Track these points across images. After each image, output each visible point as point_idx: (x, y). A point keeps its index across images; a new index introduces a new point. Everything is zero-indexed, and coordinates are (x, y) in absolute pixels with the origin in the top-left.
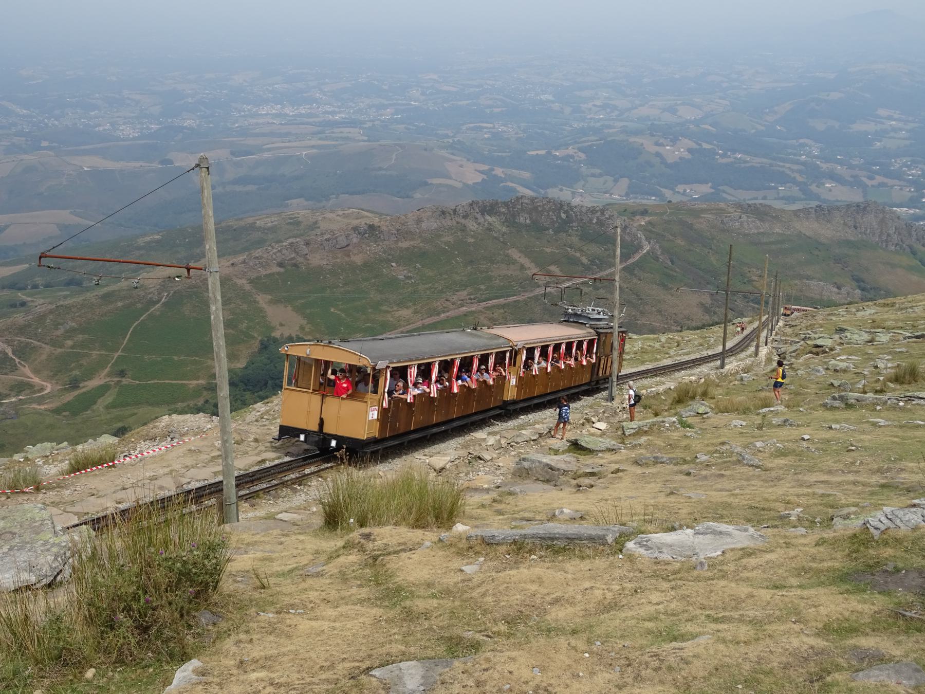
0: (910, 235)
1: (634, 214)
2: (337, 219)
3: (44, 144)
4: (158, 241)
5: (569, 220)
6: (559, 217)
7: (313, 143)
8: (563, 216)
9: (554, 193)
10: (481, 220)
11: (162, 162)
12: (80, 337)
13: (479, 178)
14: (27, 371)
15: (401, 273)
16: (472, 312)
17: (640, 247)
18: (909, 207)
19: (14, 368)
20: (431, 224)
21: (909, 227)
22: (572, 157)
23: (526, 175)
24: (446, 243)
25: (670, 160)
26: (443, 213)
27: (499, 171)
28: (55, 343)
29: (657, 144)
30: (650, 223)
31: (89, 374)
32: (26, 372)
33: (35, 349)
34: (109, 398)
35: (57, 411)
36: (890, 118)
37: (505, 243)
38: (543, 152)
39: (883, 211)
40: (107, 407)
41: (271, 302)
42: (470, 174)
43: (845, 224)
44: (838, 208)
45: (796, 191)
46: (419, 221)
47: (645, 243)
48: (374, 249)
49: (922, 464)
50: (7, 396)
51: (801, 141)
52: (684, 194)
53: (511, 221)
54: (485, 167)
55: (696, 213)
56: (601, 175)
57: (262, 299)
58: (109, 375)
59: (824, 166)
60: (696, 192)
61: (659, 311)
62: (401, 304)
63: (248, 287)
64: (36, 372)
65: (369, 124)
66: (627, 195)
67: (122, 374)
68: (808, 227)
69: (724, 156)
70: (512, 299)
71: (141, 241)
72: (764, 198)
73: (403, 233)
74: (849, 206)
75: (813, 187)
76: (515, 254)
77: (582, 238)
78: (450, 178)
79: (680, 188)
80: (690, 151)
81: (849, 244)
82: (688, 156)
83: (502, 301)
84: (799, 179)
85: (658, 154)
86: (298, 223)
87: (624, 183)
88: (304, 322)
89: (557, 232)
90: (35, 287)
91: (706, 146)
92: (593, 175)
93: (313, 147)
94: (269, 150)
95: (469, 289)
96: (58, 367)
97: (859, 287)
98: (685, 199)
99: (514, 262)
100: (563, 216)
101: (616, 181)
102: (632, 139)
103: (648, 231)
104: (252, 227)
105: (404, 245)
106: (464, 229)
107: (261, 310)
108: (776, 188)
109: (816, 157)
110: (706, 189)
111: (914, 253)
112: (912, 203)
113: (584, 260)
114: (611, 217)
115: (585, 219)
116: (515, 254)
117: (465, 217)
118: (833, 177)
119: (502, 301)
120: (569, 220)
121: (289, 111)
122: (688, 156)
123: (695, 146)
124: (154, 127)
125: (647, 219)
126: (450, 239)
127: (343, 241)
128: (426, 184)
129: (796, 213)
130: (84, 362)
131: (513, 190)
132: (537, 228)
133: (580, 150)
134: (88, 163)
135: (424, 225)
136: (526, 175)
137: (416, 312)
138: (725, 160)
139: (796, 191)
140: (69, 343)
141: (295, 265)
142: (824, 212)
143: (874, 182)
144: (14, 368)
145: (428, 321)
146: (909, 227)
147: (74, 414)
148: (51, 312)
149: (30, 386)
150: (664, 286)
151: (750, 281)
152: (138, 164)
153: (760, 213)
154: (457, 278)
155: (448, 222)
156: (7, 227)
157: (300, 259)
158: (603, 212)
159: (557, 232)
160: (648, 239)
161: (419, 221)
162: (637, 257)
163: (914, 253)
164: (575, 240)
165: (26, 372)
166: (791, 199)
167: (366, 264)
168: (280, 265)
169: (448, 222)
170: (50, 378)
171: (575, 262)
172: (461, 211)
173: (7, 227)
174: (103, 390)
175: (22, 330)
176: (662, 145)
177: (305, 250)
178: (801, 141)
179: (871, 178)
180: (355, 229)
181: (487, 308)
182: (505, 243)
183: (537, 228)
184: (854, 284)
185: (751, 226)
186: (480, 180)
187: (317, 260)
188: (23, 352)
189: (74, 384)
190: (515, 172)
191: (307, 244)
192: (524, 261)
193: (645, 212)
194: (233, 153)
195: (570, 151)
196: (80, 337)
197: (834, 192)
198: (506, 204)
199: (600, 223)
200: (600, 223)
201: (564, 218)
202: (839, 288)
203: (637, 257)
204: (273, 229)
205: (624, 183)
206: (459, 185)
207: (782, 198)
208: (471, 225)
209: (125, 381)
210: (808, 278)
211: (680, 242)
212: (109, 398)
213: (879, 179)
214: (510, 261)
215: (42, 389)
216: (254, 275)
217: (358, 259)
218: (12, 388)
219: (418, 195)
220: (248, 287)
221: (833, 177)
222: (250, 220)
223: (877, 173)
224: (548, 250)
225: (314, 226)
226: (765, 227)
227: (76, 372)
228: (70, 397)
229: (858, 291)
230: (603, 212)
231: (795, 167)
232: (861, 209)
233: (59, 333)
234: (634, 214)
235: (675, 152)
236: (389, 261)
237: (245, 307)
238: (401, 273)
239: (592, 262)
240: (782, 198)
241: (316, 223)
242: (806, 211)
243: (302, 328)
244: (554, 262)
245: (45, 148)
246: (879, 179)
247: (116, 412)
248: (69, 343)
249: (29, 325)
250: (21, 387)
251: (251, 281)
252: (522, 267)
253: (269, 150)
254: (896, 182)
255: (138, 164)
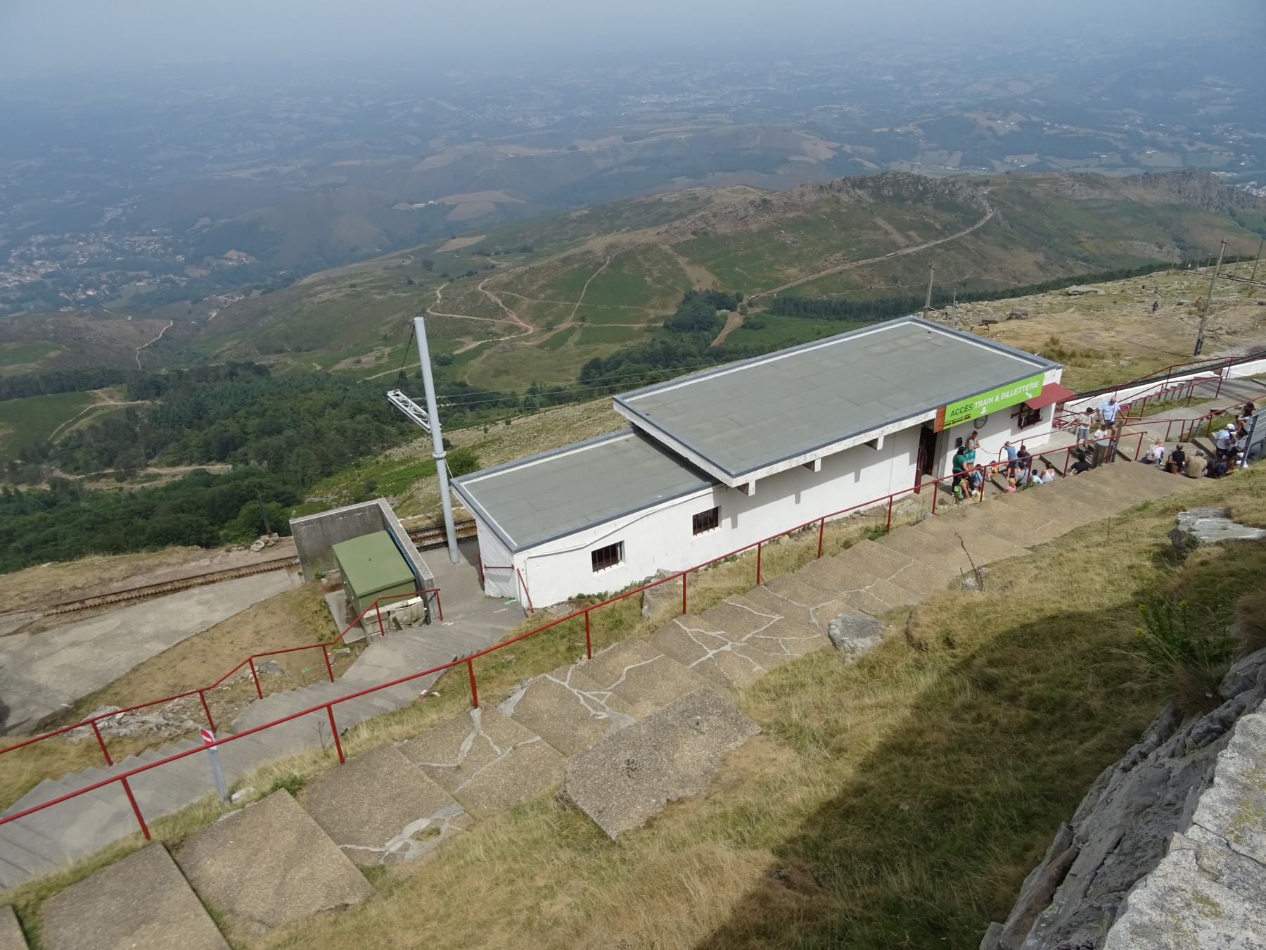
0: (1231, 198)
1: (977, 184)
2: (732, 193)
3: (474, 136)
4: (587, 216)
5: (925, 192)
6: (917, 189)
7: (689, 127)
8: (920, 188)
9: (895, 166)
10: (852, 193)
11: (569, 149)
12: (549, 292)
13: (830, 154)
14: (514, 316)
15: (788, 238)
16: (846, 271)
17: (985, 214)
18: (1227, 171)
19: (505, 315)
20: (811, 198)
21: (1231, 190)
22: (912, 133)
23: (871, 150)
24: (824, 213)
25: (1001, 134)
26: (821, 187)
27: (848, 148)
28: (531, 296)
29: (990, 118)
30: (992, 192)
31: (560, 319)
32: (514, 318)
33: (517, 300)
34: (576, 337)
35: (541, 346)
36: (1216, 85)
37: (872, 213)
38: (886, 130)
39: (1208, 176)
40: (576, 344)
41: (689, 263)
42: (824, 151)
43: (1170, 189)
44: (1164, 175)
45: (1117, 159)
46: (802, 195)
47: (988, 209)
48: (767, 219)
49: (723, 949)
50: (502, 336)
51: (1126, 110)
52: (1012, 164)
53: (876, 194)
54: (836, 145)
55: (1033, 183)
56: (937, 149)
57: (682, 261)
58: (574, 320)
59: (1147, 134)
60: (1024, 161)
61: (1000, 269)
62: (790, 264)
63: (670, 252)
64: (521, 317)
65: (734, 110)
66: (960, 166)
67: (583, 319)
68: (1134, 193)
69: (1052, 127)
70: (877, 259)
71: (574, 216)
72: (1087, 166)
73: (790, 206)
74: (1175, 173)
75: (1135, 155)
76: (880, 221)
77: (938, 206)
78: (805, 155)
79: (1008, 159)
80: (1020, 124)
81: (1172, 207)
82: (1018, 129)
83: (870, 261)
84: (1122, 147)
85: (990, 128)
86: (696, 198)
87: (958, 155)
88: (715, 279)
89: (915, 202)
90: (497, 253)
91: (1034, 119)
92: (930, 149)
93: (689, 131)
94: (654, 135)
95: (843, 252)
96: (536, 314)
97: (1178, 246)
98: (1013, 169)
99: (880, 228)
100: (920, 188)
101: (950, 154)
102: (966, 115)
103: (991, 198)
104: (659, 202)
105: (791, 215)
106: (838, 201)
107: (681, 270)
108: (1098, 156)
109: (1138, 125)
110: (1033, 159)
111: (1233, 214)
112: (1229, 167)
113: (938, 226)
114: (961, 188)
115: (939, 190)
116: (880, 221)
117: (839, 191)
118: (1155, 144)
119: (870, 261)
120: (925, 192)
121: (666, 99)
122: (1018, 129)
123: (1023, 119)
124: (558, 118)
125: (990, 189)
126: (827, 210)
127: (742, 213)
128: (787, 161)
129: (1124, 180)
130: (555, 310)
131: (861, 165)
132: (899, 199)
133: (920, 126)
134: (511, 151)
135: (806, 199)
136: (871, 150)
137: (801, 270)
138: (1053, 132)
139: (1117, 159)
140: (542, 296)
141: (706, 234)
142: (1149, 178)
143: (1194, 148)
144: (505, 315)
145: (811, 278)
146: (1231, 190)
147: (553, 349)
148: (526, 272)
149: (518, 328)
150: (1006, 248)
151: (1080, 243)
152: (550, 151)
153: (1091, 181)
154: (834, 242)
155: (825, 195)
156: (456, 205)
157: (709, 229)
158: (954, 183)
159: (915, 202)
160: (992, 207)
161: (802, 195)
162: (982, 223)
163: (1233, 214)
164: (930, 208)
165: (514, 318)
166: (1112, 167)
167: (761, 232)
168: (694, 233)
169: (825, 195)
170: (531, 322)
171: (928, 227)
172: (836, 185)
173: (456, 205)
174: (571, 331)
175: (507, 286)
176: (994, 119)
177: (713, 221)
178: (1126, 110)
179: (1191, 144)
180: (752, 203)
181: (858, 267)
182: (872, 213)
183: (899, 199)
184: (1174, 243)
185: (1083, 193)
186: (830, 156)
187: (724, 229)
188: (510, 303)
189: (549, 327)
190: (862, 148)
191: (714, 216)
192: (888, 227)
193: (986, 183)
194: (625, 139)
195: (911, 127)
196: (549, 292)
197: (1154, 159)
198: (873, 179)
199: (952, 193)
200: (952, 193)
201: (919, 190)
202: (1160, 247)
203: (982, 223)
204: (677, 204)
205: (958, 155)
206: (815, 161)
207: (1103, 166)
208: (844, 197)
209: (586, 325)
210: (1132, 239)
211: (1019, 209)
212: (576, 337)
213: (1200, 145)
214: (877, 228)
215: (527, 331)
216: (674, 242)
217: (754, 228)
218: (505, 330)
219: (780, 172)
220: (670, 252)
221: (1155, 144)
222: (657, 197)
223: (1197, 139)
224: (908, 218)
225: (709, 200)
226: (1095, 194)
227: (550, 318)
228: (548, 336)
229: (1178, 251)
230: (954, 183)
231: (1119, 136)
232: (1187, 175)
233: (534, 288)
234: (977, 184)
235: (1006, 126)
236: (779, 229)
237: (669, 267)
238: (788, 238)
239: (945, 228)
240: (1103, 166)
241: (710, 197)
242: (1134, 178)
243: (714, 284)
244: (913, 228)
245: (475, 140)
246: (1200, 145)
247: (583, 347)
248: (542, 296)
249: (512, 282)
250: (511, 329)
251: (673, 247)
252: (886, 233)
253: (654, 135)
254: (1217, 147)
255: (550, 151)
